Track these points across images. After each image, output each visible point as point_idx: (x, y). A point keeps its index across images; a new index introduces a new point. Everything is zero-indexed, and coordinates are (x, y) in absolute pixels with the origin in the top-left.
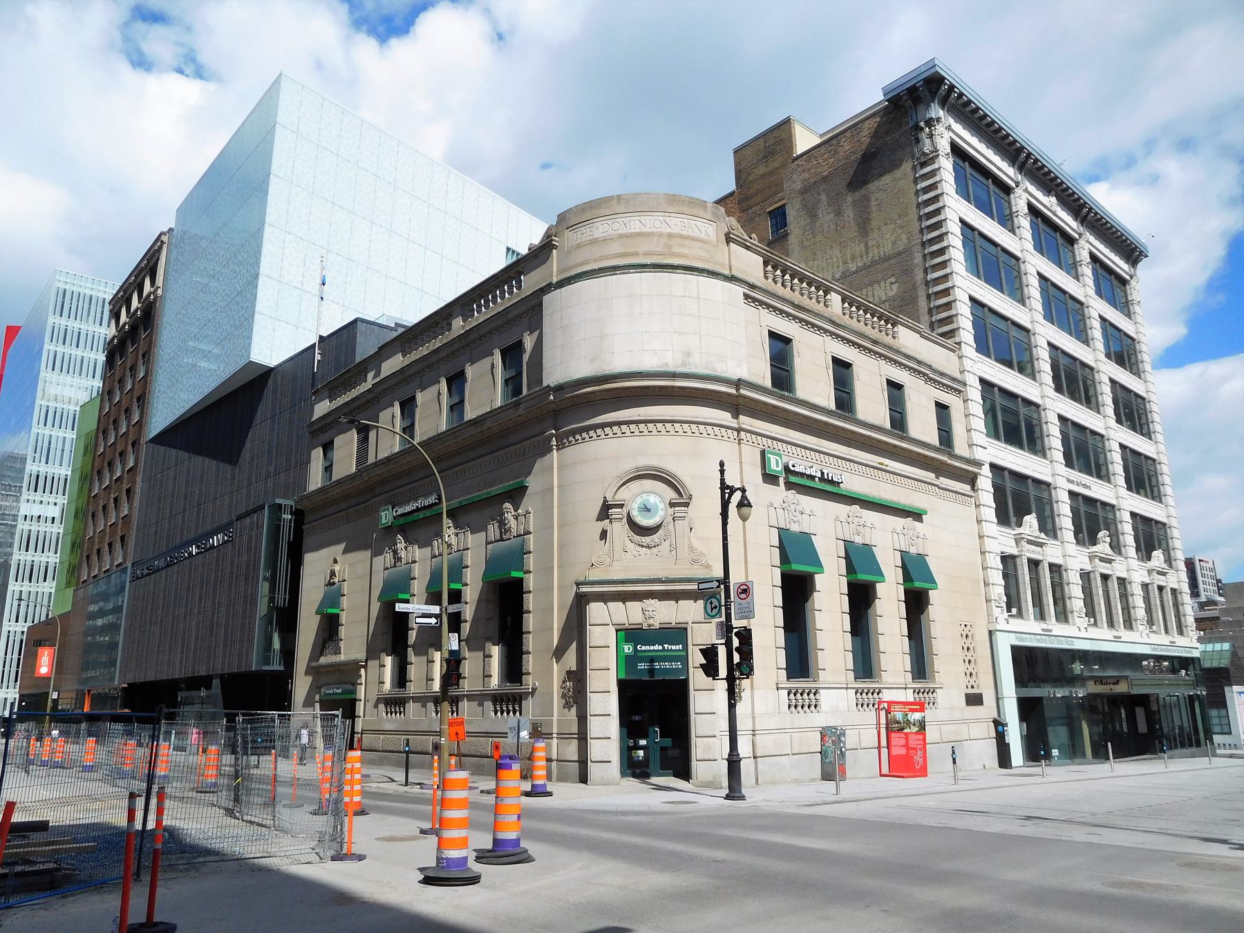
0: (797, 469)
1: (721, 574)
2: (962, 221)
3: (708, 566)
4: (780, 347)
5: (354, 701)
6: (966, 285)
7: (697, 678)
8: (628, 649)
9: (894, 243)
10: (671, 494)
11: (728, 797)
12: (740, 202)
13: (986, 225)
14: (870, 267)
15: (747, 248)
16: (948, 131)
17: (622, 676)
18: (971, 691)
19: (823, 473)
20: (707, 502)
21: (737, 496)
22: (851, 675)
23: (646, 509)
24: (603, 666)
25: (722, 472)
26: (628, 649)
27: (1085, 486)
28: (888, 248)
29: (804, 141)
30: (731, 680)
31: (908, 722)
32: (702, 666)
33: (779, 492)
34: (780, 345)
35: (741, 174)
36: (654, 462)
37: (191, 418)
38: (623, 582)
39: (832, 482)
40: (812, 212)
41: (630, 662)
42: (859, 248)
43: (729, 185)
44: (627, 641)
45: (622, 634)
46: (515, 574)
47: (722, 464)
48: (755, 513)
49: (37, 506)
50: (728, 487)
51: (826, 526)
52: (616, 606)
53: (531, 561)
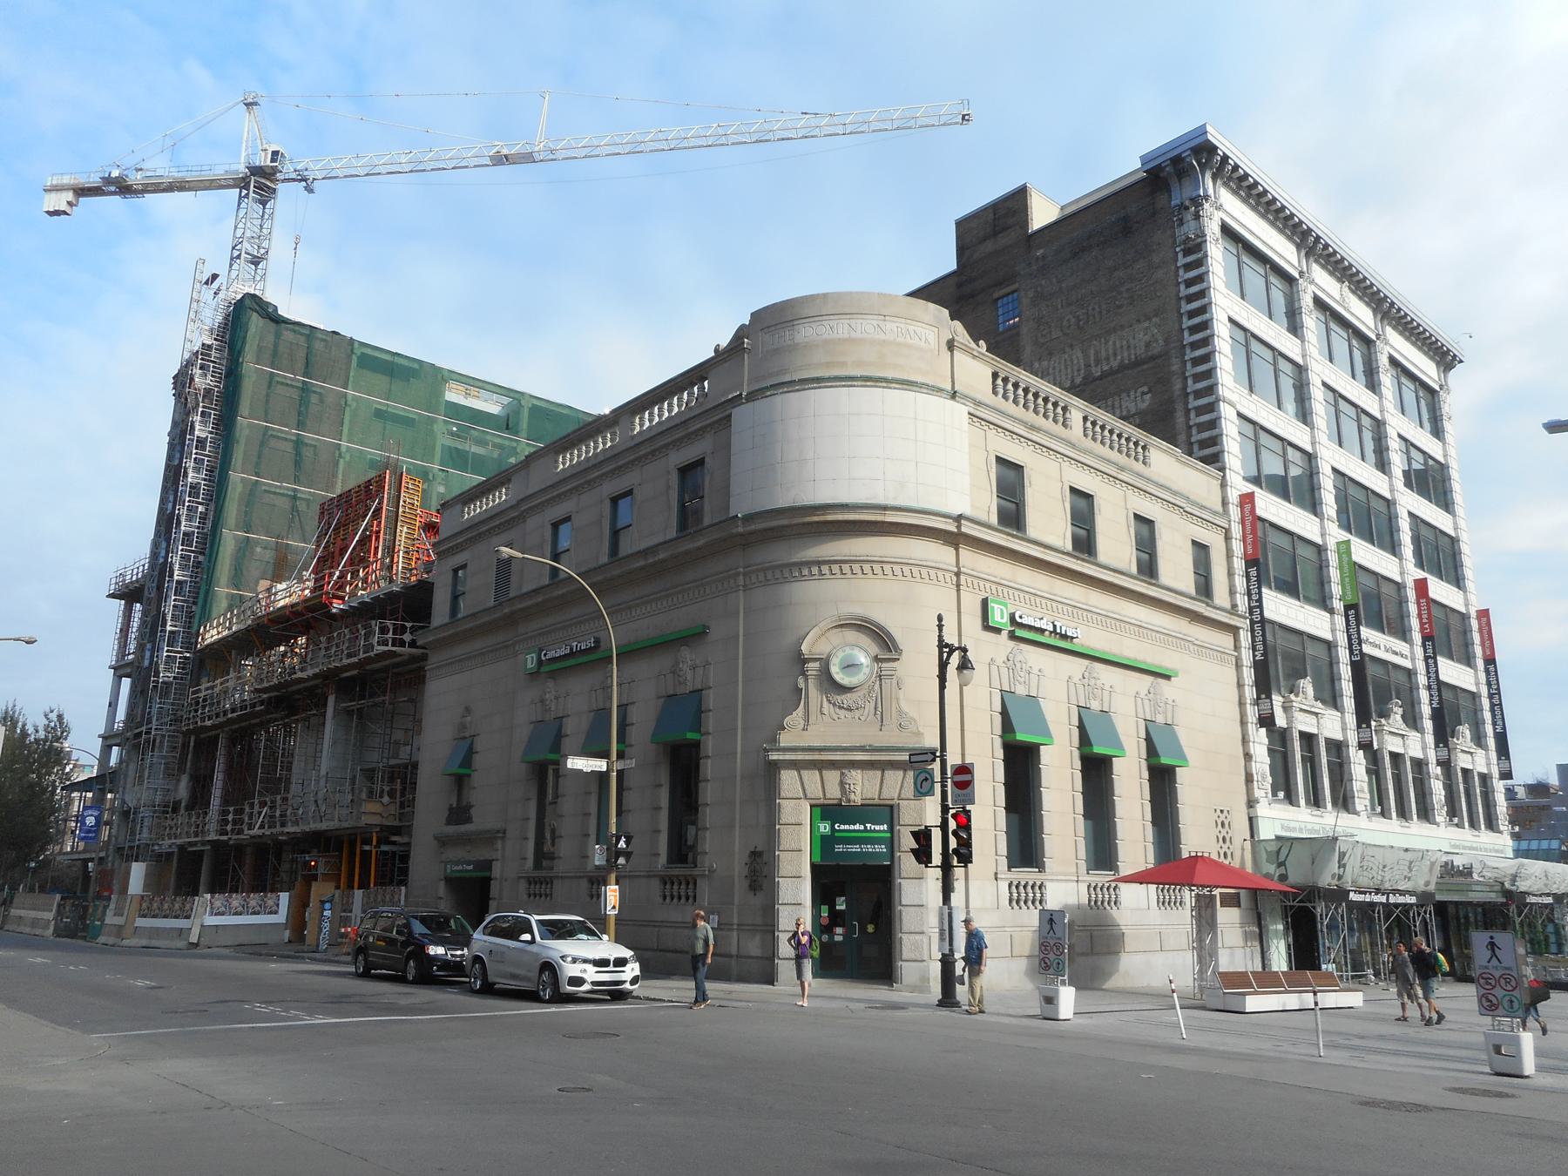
0: (1025, 621)
1: (936, 744)
2: (1231, 320)
3: (919, 734)
4: (1010, 483)
5: (488, 880)
6: (1235, 397)
7: (908, 863)
8: (824, 828)
10: (874, 649)
11: (942, 1004)
12: (959, 285)
14: (1117, 372)
15: (974, 357)
16: (1225, 207)
17: (817, 859)
20: (919, 661)
21: (955, 659)
22: (1004, 862)
23: (850, 666)
24: (794, 846)
25: (940, 627)
26: (824, 828)
29: (1042, 214)
30: (946, 868)
32: (913, 851)
33: (1001, 646)
34: (1011, 474)
35: (962, 250)
36: (859, 610)
39: (1064, 637)
41: (826, 843)
43: (947, 262)
44: (823, 819)
45: (818, 810)
46: (691, 736)
47: (940, 618)
48: (979, 674)
50: (947, 645)
52: (812, 777)
53: (710, 722)
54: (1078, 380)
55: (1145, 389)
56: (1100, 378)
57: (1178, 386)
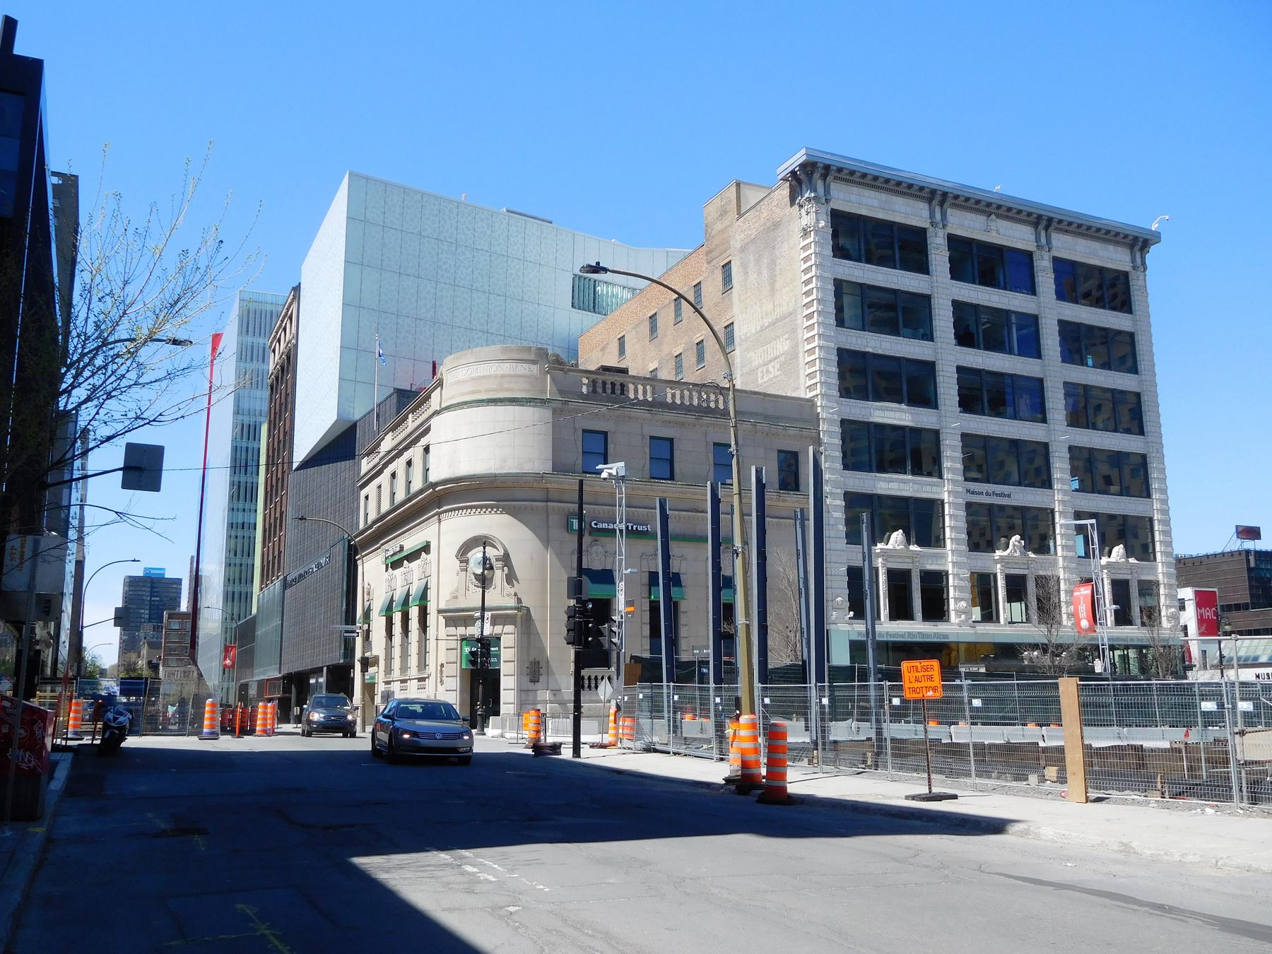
27: (1002, 495)
38: (463, 610)
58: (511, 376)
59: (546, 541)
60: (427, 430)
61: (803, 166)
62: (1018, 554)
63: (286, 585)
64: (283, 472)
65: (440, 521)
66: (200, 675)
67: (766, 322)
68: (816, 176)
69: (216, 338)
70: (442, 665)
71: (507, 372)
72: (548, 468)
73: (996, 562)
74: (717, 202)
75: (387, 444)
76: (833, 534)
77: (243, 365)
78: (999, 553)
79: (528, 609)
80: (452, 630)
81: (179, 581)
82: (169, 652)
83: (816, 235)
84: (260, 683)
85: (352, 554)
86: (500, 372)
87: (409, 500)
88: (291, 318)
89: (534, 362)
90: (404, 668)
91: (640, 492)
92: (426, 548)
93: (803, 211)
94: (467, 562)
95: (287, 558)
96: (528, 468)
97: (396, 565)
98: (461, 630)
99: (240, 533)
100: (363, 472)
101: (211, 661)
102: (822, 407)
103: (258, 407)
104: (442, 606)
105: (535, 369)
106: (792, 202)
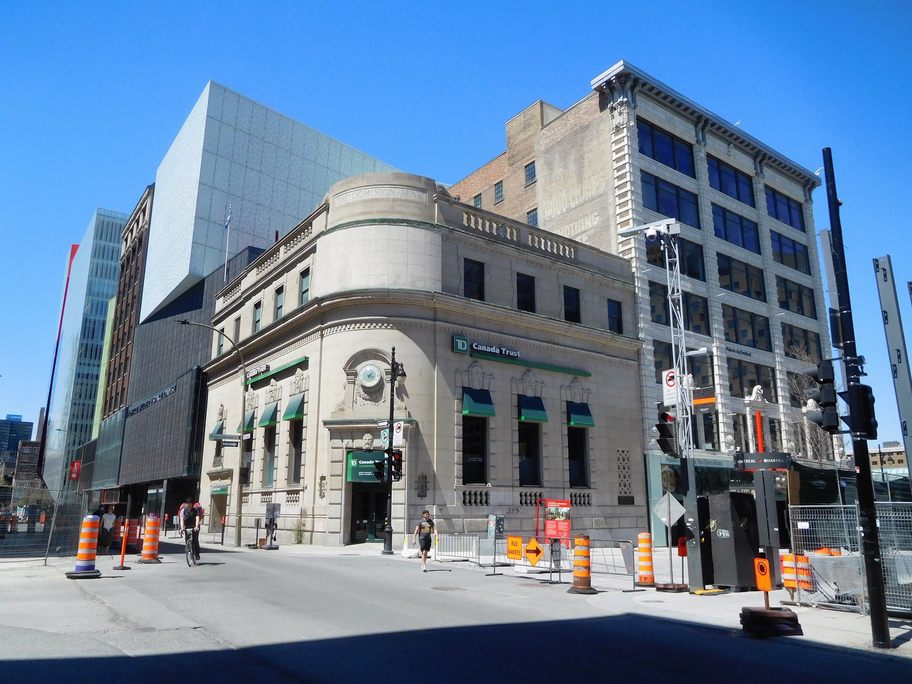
5: (227, 495)
8: (353, 463)
9: (598, 188)
13: (668, 174)
17: (349, 480)
18: (623, 495)
19: (501, 351)
23: (370, 376)
26: (353, 463)
27: (746, 354)
28: (594, 192)
31: (558, 514)
37: (160, 311)
38: (351, 422)
40: (550, 165)
42: (577, 192)
44: (353, 458)
49: (86, 368)
51: (503, 384)
54: (564, 210)
55: (596, 214)
56: (574, 209)
57: (612, 211)
58: (402, 200)
59: (434, 359)
60: (313, 250)
61: (619, 76)
62: (760, 400)
63: (127, 414)
64: (130, 327)
65: (322, 336)
66: (44, 485)
67: (573, 205)
68: (629, 84)
69: (75, 249)
70: (323, 478)
71: (399, 196)
72: (437, 287)
73: (746, 405)
74: (520, 119)
75: (220, 304)
76: (647, 373)
77: (96, 260)
78: (747, 399)
79: (417, 424)
80: (337, 443)
81: (31, 424)
82: (20, 469)
83: (628, 131)
84: (103, 492)
85: (201, 383)
86: (392, 196)
87: (301, 310)
88: (144, 211)
89: (423, 191)
90: (268, 478)
91: (511, 321)
92: (304, 364)
93: (616, 113)
94: (356, 375)
95: (129, 393)
96: (421, 286)
97: (256, 385)
98: (348, 443)
99: (85, 381)
100: (217, 310)
101: (54, 477)
102: (637, 268)
103: (105, 292)
104: (328, 418)
105: (424, 197)
106: (603, 107)
